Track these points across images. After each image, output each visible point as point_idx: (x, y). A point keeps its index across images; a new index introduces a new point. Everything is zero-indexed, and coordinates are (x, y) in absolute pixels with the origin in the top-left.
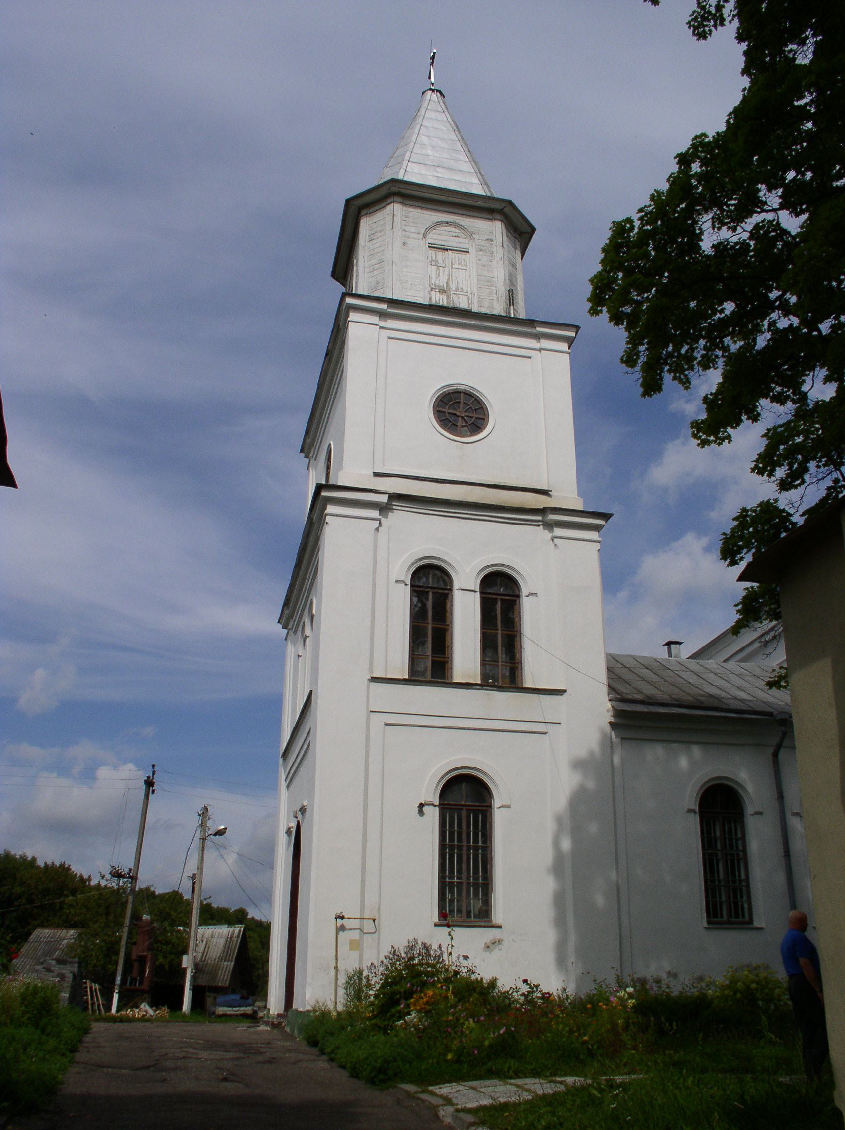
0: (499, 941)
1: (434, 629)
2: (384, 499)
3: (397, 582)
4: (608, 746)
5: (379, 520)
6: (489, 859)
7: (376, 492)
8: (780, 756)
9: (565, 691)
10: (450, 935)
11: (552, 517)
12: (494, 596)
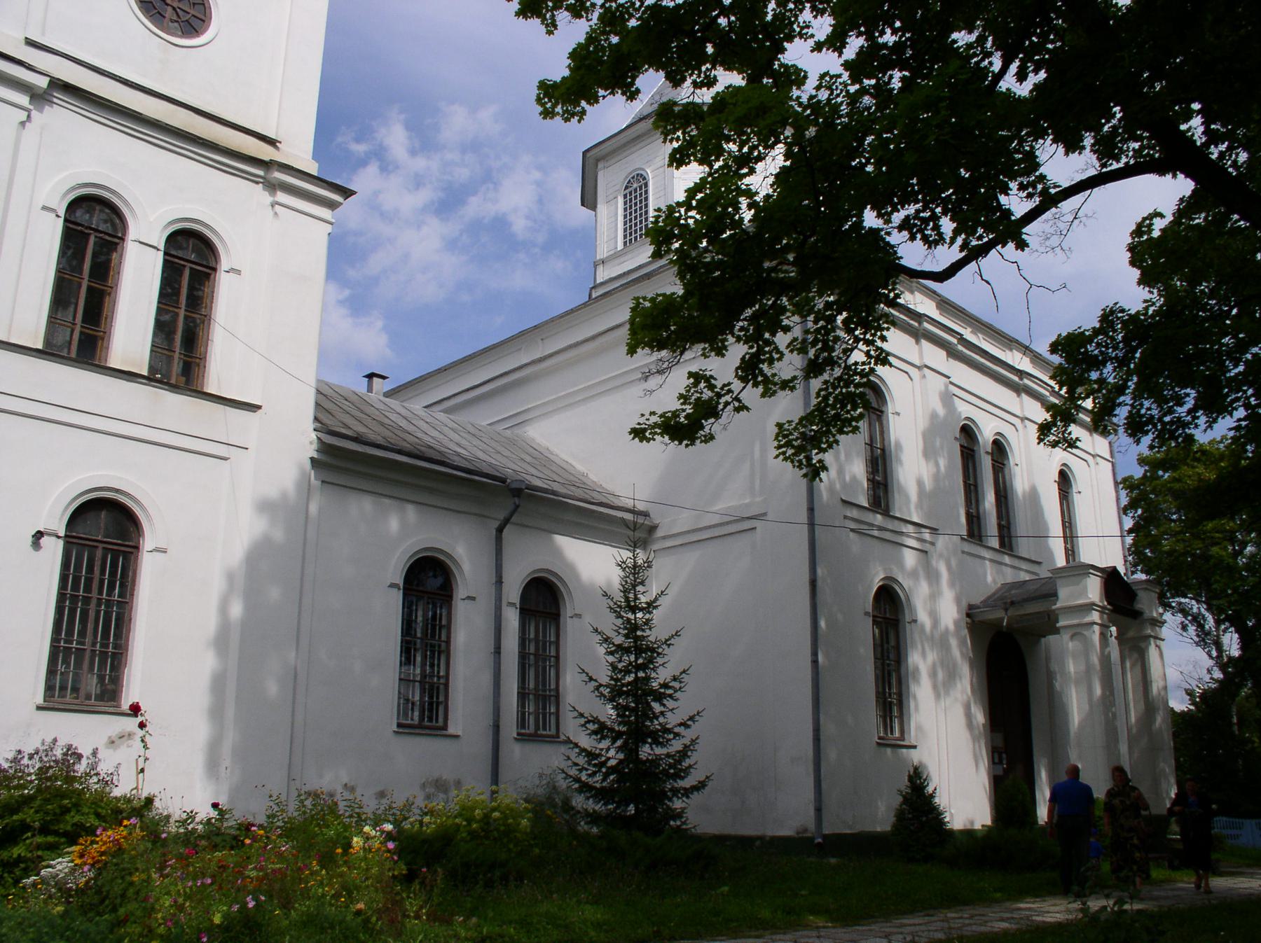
0: (129, 735)
1: (90, 289)
2: (43, 82)
3: (45, 208)
4: (305, 491)
5: (28, 111)
6: (126, 618)
7: (30, 68)
8: (505, 531)
9: (259, 407)
10: (143, 741)
11: (278, 175)
12: (182, 262)
